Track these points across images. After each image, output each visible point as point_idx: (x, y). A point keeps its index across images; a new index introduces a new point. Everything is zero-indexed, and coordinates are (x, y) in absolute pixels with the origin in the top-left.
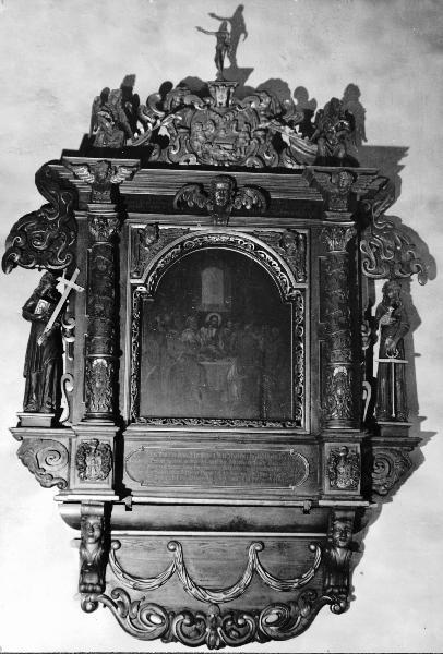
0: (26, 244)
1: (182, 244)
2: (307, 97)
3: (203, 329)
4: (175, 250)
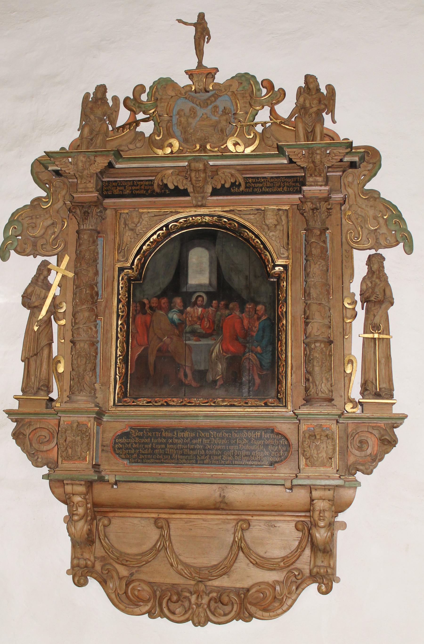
0: (26, 232)
1: (167, 226)
2: (38, 199)
3: (189, 309)
4: (161, 232)
